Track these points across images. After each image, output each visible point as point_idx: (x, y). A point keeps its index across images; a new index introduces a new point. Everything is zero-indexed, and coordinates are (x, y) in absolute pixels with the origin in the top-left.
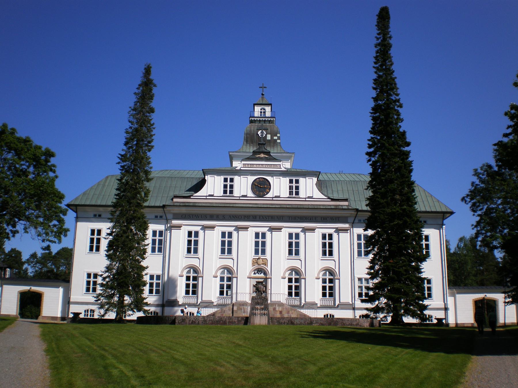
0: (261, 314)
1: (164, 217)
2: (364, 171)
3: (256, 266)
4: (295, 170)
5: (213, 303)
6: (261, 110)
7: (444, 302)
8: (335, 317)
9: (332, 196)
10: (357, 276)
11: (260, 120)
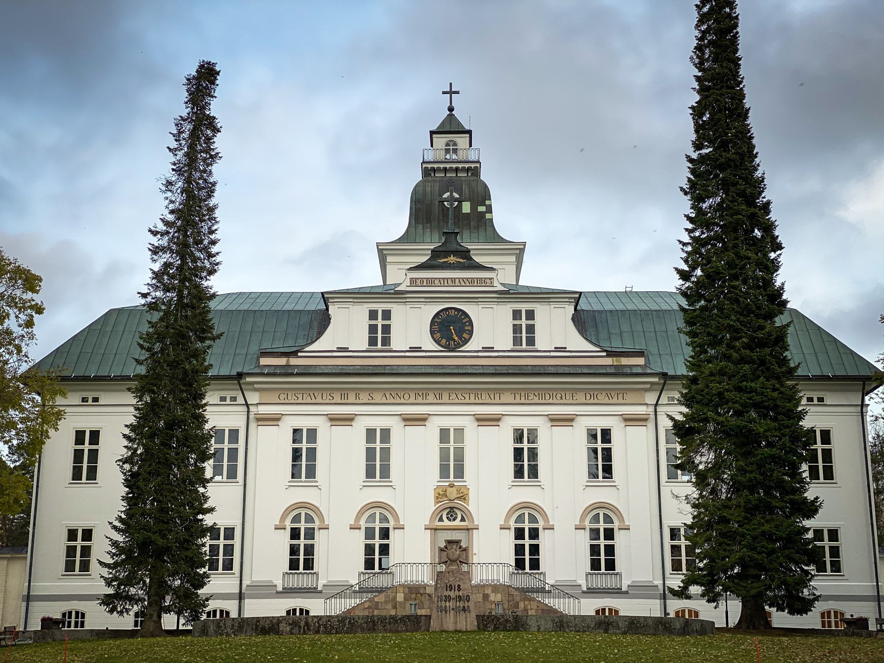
3: (445, 503)
6: (447, 145)
8: (621, 614)
9: (608, 345)
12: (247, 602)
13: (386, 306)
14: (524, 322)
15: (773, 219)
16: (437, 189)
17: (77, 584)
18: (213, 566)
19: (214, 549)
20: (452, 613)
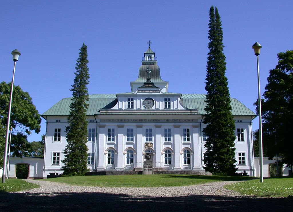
0: (149, 170)
2: (203, 95)
4: (171, 93)
15: (225, 72)
20: (148, 170)
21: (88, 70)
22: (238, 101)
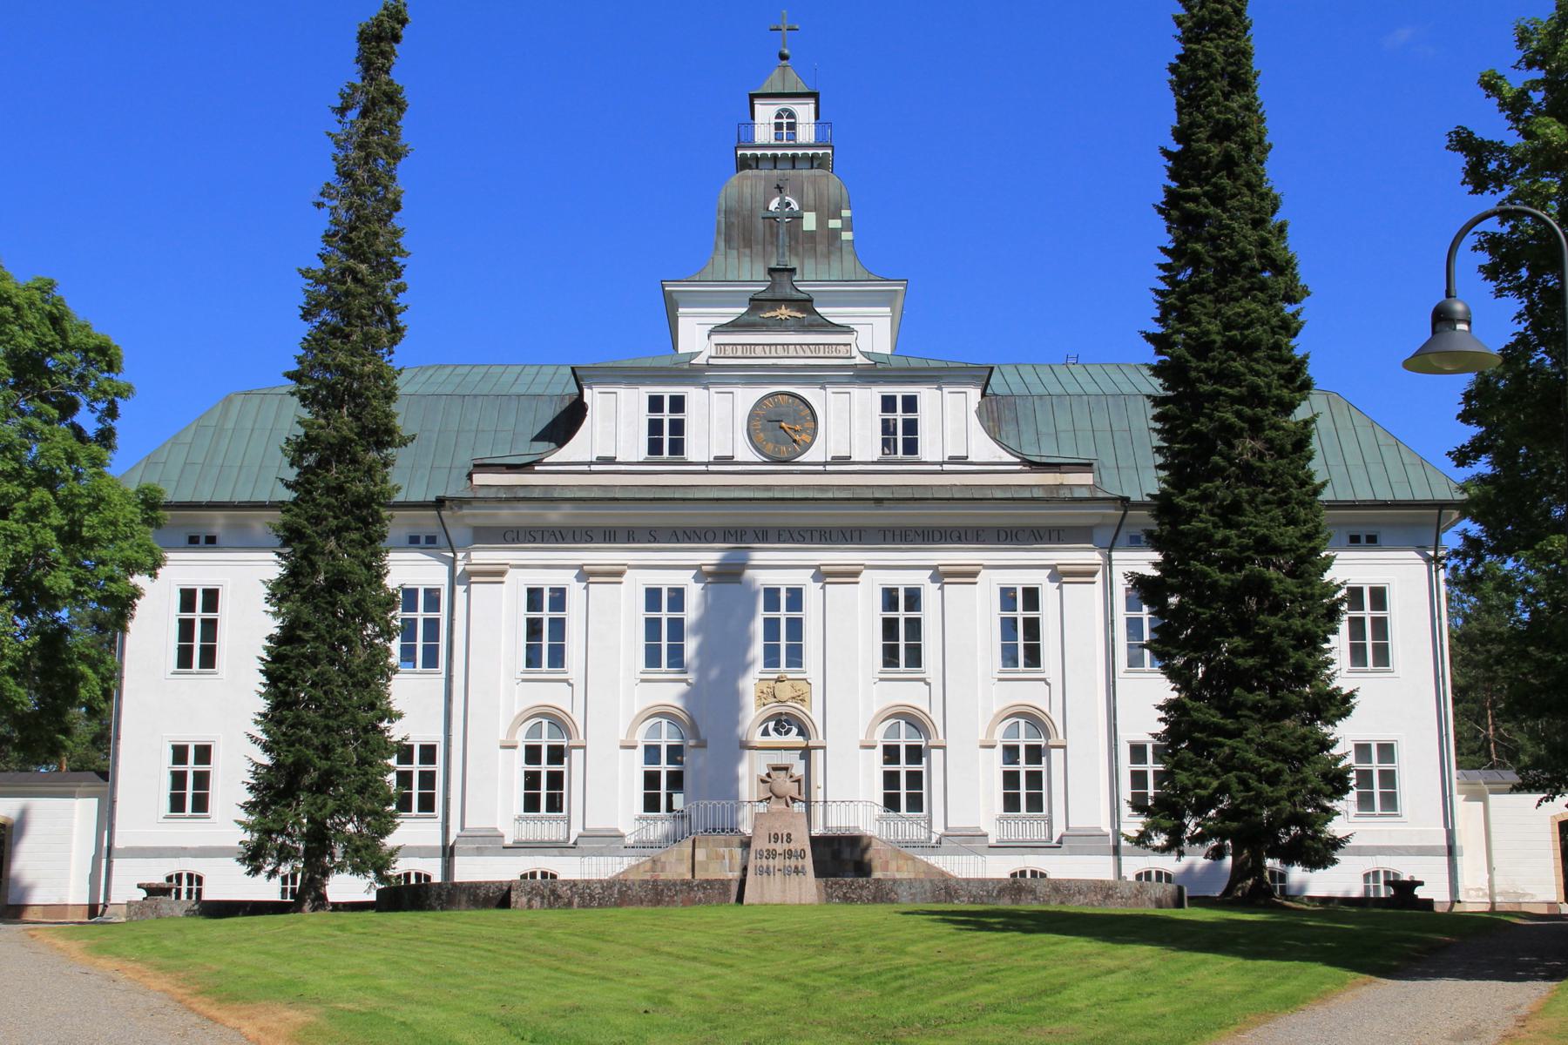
1: (441, 540)
4: (923, 364)
5: (622, 836)
6: (779, 116)
7: (1446, 825)
9: (1036, 452)
10: (1126, 737)
11: (775, 157)
12: (459, 861)
13: (677, 390)
14: (899, 416)
16: (761, 189)
17: (189, 831)
18: (405, 805)
19: (405, 778)
21: (395, 155)
22: (1353, 410)
